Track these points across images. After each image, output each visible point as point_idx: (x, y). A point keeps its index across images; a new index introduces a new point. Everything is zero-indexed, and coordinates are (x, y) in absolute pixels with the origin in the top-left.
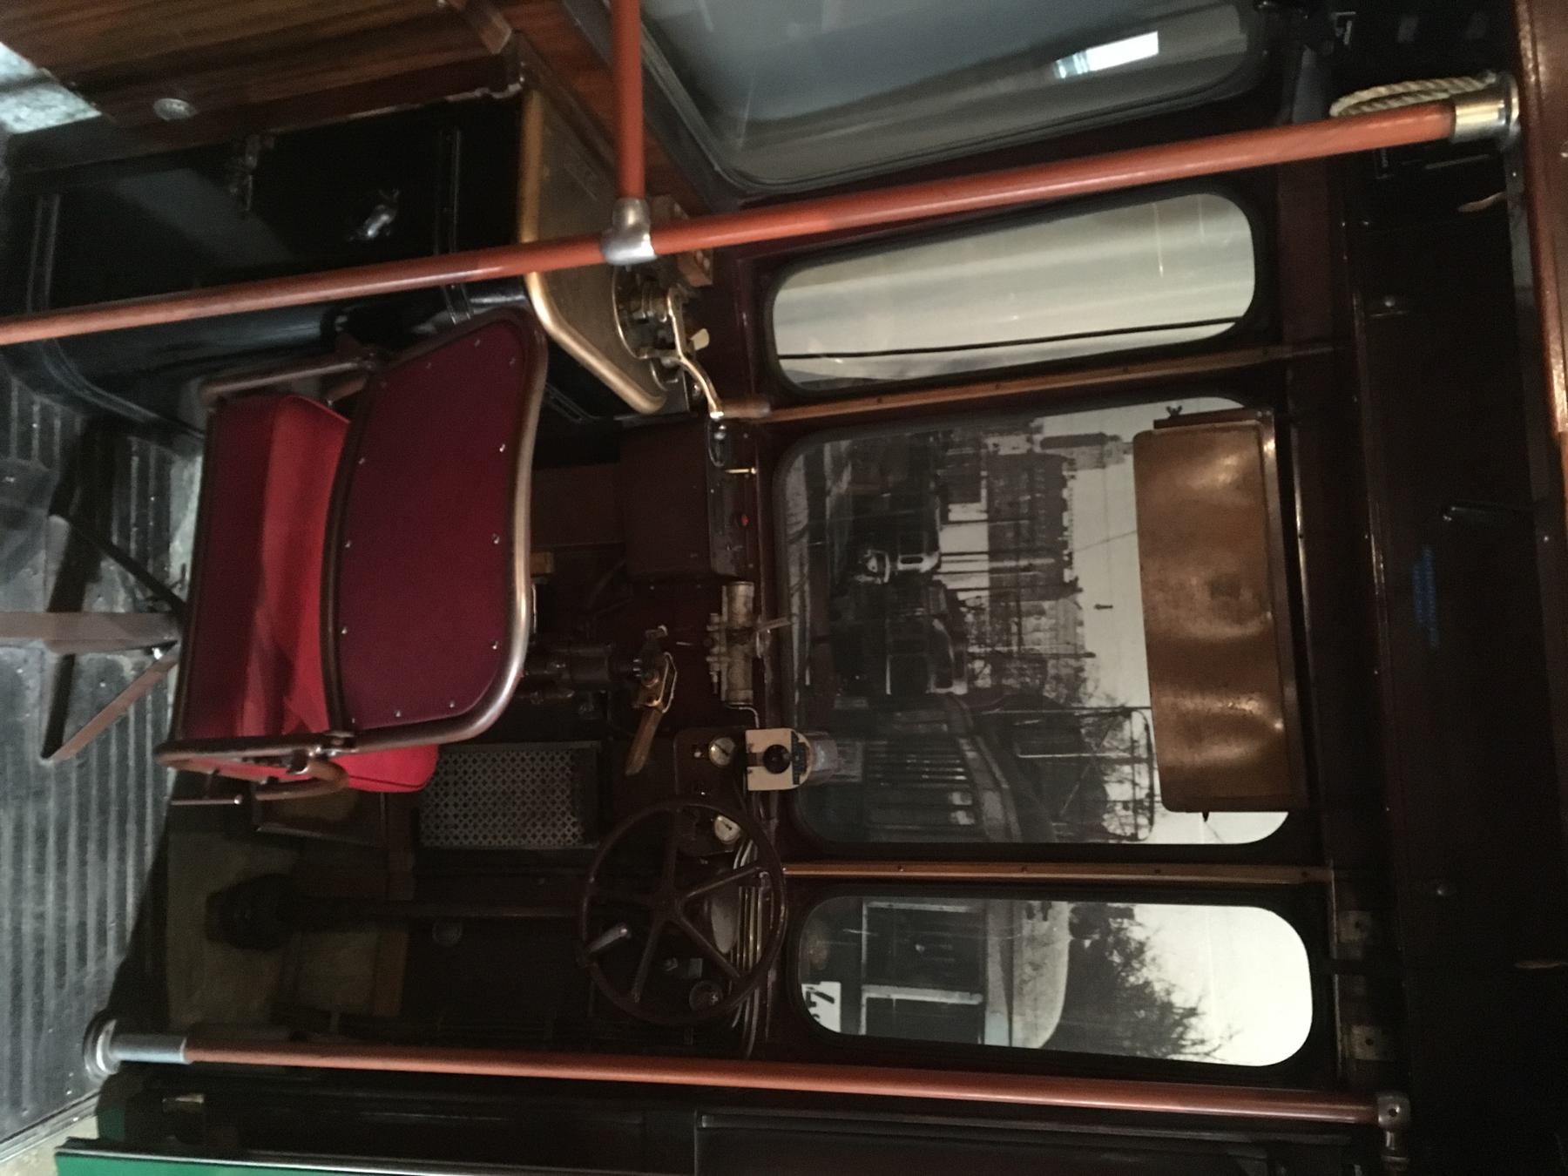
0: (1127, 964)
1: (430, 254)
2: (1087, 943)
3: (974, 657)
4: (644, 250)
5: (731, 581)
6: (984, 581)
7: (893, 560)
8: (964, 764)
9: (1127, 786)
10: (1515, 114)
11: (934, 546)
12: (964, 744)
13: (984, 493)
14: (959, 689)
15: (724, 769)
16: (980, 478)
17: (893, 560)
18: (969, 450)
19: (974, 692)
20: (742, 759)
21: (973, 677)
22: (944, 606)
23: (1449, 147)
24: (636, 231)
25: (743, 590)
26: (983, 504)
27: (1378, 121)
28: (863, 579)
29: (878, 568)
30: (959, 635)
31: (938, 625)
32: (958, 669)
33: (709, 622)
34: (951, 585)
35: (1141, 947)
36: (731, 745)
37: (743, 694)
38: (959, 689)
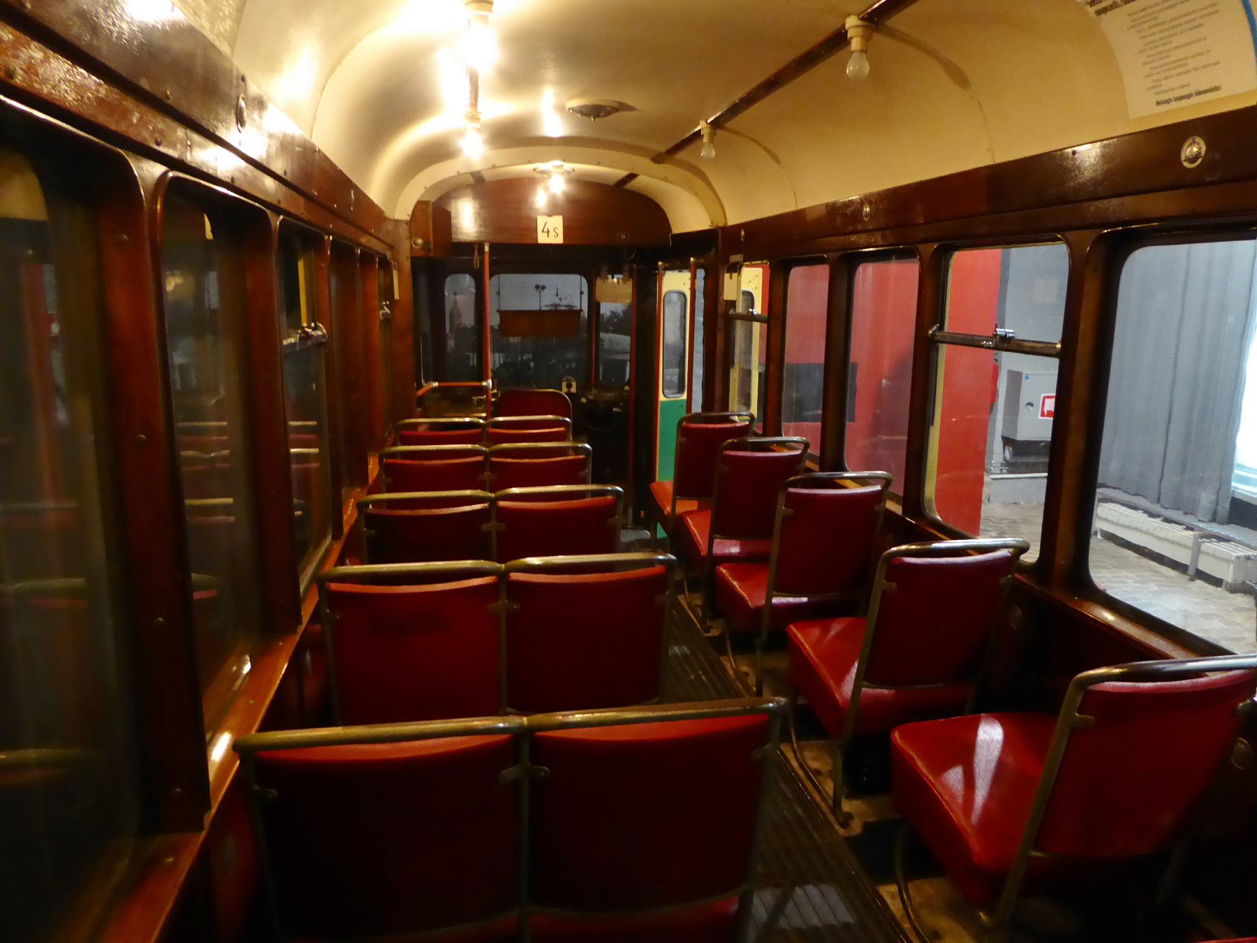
4: (490, 381)
14: (532, 364)
19: (534, 359)
32: (526, 363)
38: (532, 364)
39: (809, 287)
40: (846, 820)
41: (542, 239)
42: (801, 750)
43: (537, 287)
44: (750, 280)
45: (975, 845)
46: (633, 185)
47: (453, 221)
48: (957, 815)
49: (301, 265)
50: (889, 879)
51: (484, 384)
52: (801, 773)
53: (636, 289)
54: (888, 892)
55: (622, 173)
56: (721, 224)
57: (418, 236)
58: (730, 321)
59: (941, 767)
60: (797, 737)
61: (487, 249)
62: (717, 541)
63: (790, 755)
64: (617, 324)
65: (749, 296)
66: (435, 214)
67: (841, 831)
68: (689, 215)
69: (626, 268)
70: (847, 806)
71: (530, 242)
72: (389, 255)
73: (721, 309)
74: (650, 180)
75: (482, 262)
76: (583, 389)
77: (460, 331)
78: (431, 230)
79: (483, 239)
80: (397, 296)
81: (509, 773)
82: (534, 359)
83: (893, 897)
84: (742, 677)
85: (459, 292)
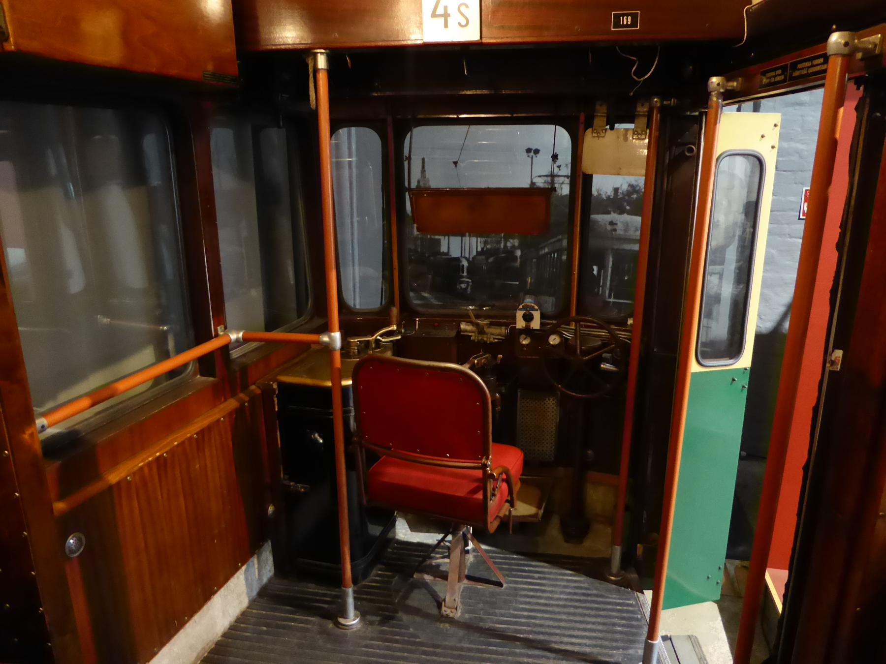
0: (637, 192)
1: (332, 419)
2: (628, 208)
3: (505, 246)
4: (337, 335)
5: (459, 331)
6: (474, 239)
7: (462, 277)
8: (550, 253)
9: (563, 186)
10: (323, 51)
11: (458, 260)
12: (542, 252)
13: (437, 237)
14: (518, 253)
15: (532, 339)
16: (431, 239)
17: (462, 277)
18: (419, 242)
19: (521, 246)
20: (527, 331)
21: (513, 246)
22: (483, 257)
23: (331, 71)
24: (330, 337)
25: (463, 326)
26: (442, 238)
27: (321, 93)
28: (469, 290)
29: (465, 284)
30: (495, 252)
31: (491, 260)
32: (510, 253)
33: (473, 341)
34: (474, 253)
35: (630, 186)
36: (523, 336)
37: (503, 330)
38: (518, 253)
43: (528, 151)
53: (658, 148)
69: (642, 109)
76: (556, 319)
82: (248, 402)
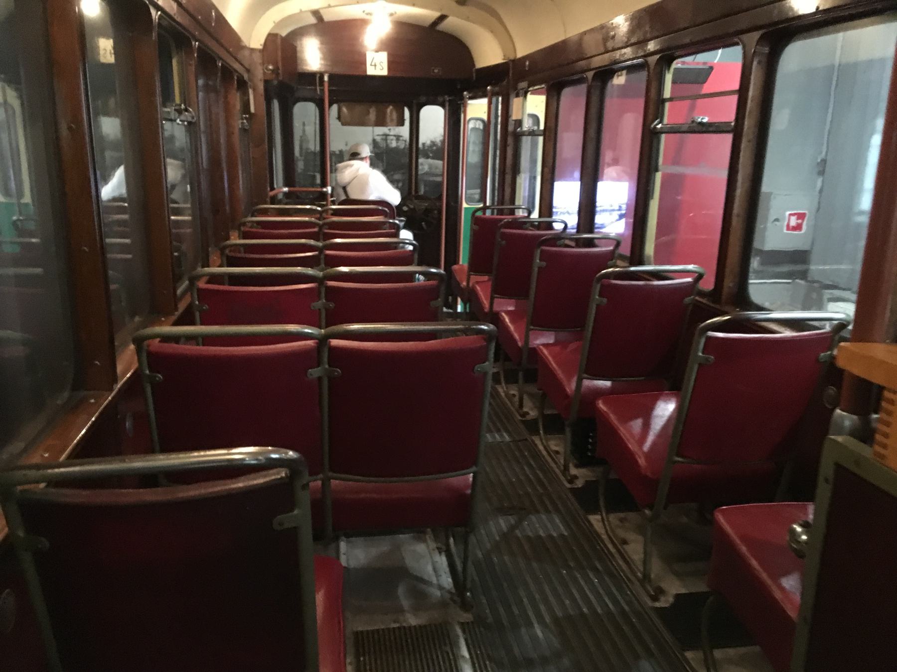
39: (573, 100)
40: (572, 479)
41: (371, 71)
42: (547, 441)
44: (535, 105)
45: (642, 461)
46: (443, 26)
47: (298, 55)
48: (632, 446)
49: (175, 62)
50: (596, 510)
51: (325, 190)
52: (544, 453)
54: (595, 519)
55: (436, 14)
56: (512, 58)
57: (269, 64)
58: (518, 137)
59: (627, 418)
60: (545, 433)
61: (326, 78)
62: (496, 301)
63: (538, 442)
64: (434, 151)
65: (535, 118)
66: (283, 47)
67: (568, 486)
68: (489, 53)
70: (573, 471)
71: (361, 73)
72: (246, 76)
73: (511, 128)
74: (455, 23)
75: (322, 91)
77: (306, 154)
78: (279, 59)
79: (323, 70)
80: (252, 110)
81: (315, 373)
83: (598, 521)
84: (510, 397)
85: (305, 114)
